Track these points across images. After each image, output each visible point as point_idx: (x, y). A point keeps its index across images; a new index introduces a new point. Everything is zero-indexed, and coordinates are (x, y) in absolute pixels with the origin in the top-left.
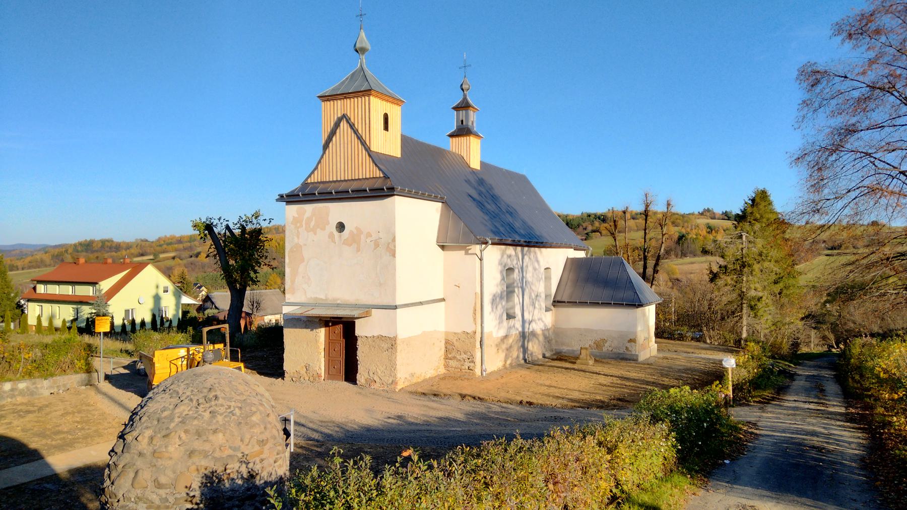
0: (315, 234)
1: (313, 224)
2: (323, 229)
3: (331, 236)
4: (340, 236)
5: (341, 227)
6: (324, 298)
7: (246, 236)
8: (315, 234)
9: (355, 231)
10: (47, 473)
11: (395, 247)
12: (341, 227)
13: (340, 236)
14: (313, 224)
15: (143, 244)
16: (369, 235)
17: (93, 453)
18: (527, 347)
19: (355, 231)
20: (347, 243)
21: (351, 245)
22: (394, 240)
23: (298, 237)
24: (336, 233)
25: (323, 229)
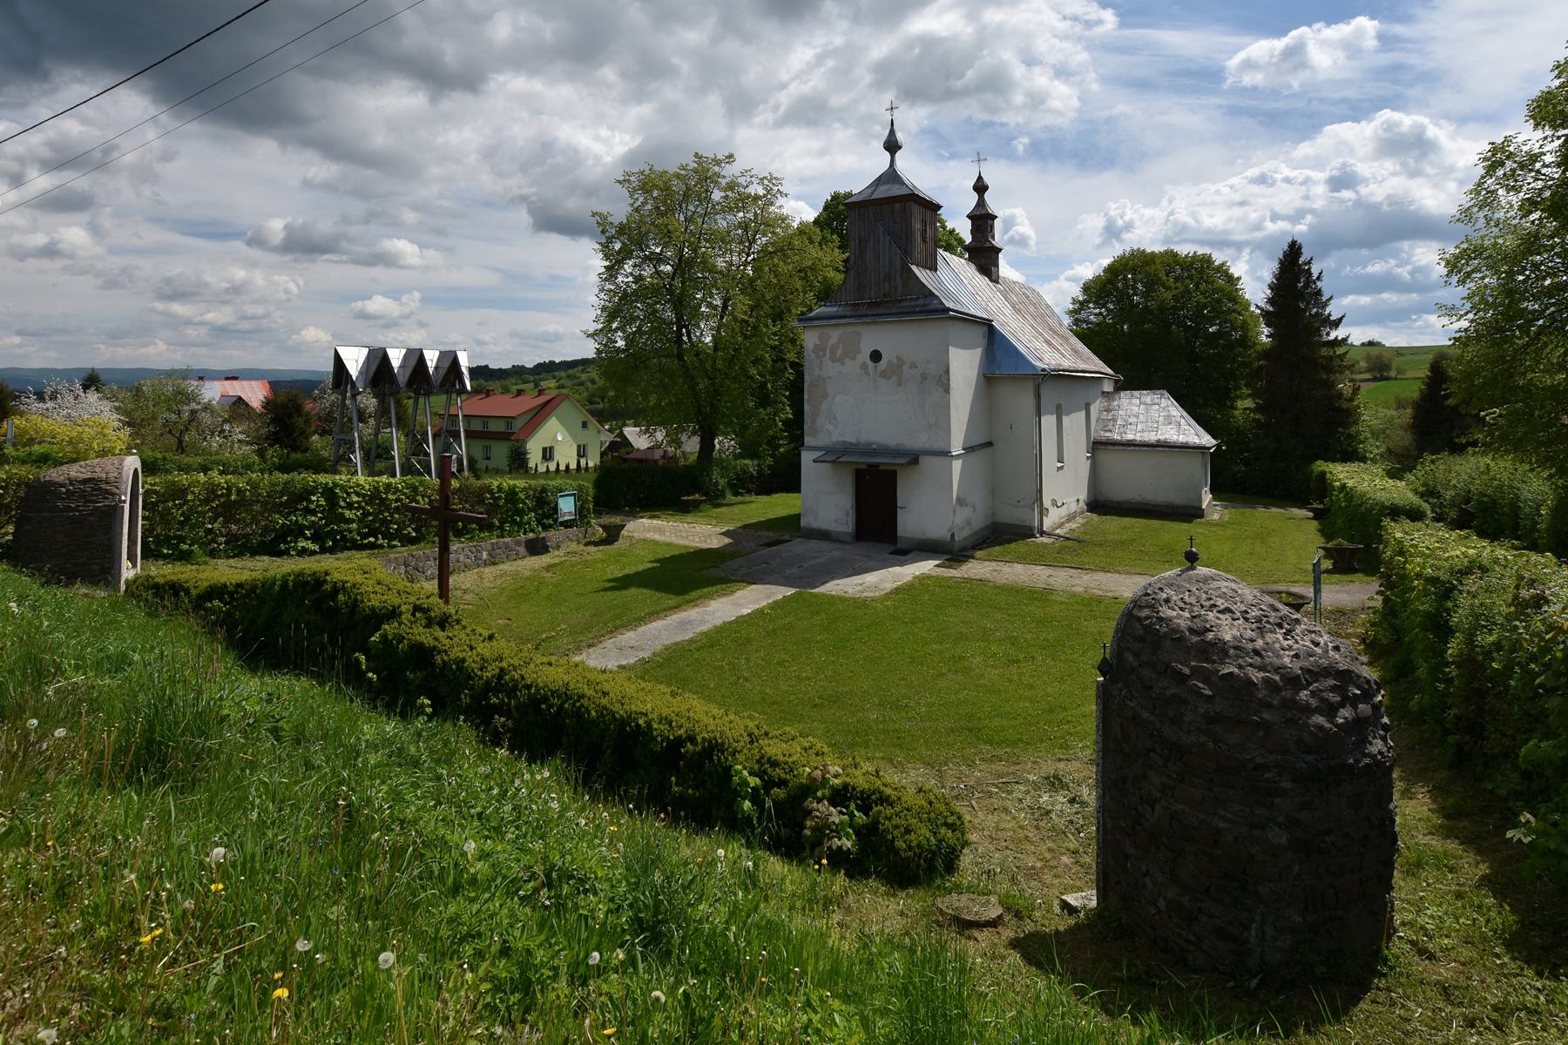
0: (843, 364)
2: (853, 359)
3: (864, 367)
4: (876, 367)
5: (876, 356)
6: (854, 441)
7: (1348, 268)
8: (843, 364)
9: (895, 361)
10: (904, 191)
11: (949, 380)
12: (876, 356)
13: (876, 367)
15: (1548, 96)
16: (913, 366)
17: (228, 571)
18: (973, 557)
19: (895, 361)
20: (884, 375)
21: (890, 377)
22: (947, 371)
23: (820, 368)
24: (871, 364)
25: (853, 359)
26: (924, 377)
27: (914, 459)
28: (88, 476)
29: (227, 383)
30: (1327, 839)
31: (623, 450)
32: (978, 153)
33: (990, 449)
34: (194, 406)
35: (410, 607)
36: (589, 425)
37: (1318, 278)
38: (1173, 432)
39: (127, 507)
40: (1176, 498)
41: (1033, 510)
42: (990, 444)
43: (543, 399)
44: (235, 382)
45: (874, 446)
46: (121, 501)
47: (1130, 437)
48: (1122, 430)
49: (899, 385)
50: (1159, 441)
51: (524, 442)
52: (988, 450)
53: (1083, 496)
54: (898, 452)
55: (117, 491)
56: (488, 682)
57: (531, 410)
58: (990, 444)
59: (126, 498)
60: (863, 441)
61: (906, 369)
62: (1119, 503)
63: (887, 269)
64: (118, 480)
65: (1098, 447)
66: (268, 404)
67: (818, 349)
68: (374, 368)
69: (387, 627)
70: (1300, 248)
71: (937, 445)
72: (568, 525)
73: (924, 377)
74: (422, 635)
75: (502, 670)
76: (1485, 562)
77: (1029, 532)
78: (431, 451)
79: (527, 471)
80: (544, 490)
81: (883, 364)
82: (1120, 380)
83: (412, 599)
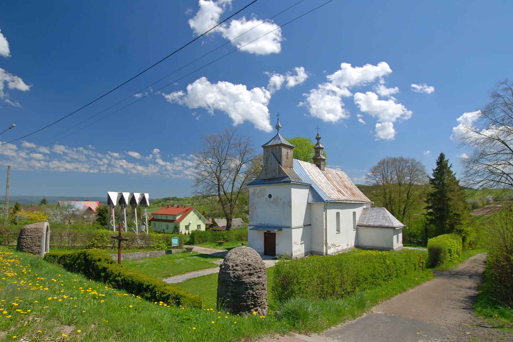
1: (259, 195)
3: (266, 199)
5: (270, 196)
9: (275, 198)
12: (270, 196)
14: (259, 195)
16: (281, 199)
19: (275, 198)
23: (254, 200)
26: (284, 203)
27: (280, 229)
28: (35, 227)
29: (86, 202)
30: (239, 295)
31: (214, 227)
32: (317, 126)
33: (310, 226)
34: (73, 209)
35: (104, 259)
36: (201, 218)
37: (450, 166)
38: (384, 222)
39: (45, 235)
40: (385, 245)
41: (323, 247)
42: (310, 225)
43: (186, 209)
44: (88, 202)
45: (269, 225)
46: (44, 234)
47: (370, 224)
48: (367, 221)
49: (277, 206)
50: (379, 225)
51: (179, 223)
52: (309, 227)
53: (353, 245)
54: (276, 227)
55: (42, 231)
56: (116, 275)
57: (183, 212)
58: (310, 225)
59: (45, 233)
60: (266, 223)
61: (279, 200)
62: (366, 246)
63: (274, 168)
64: (42, 229)
65: (358, 227)
66: (98, 209)
67: (253, 194)
68: (119, 198)
69: (157, 295)
70: (444, 155)
71: (287, 225)
72: (177, 247)
73: (284, 203)
74: (105, 265)
75: (120, 272)
76: (453, 265)
77: (321, 254)
78: (136, 224)
79: (178, 234)
80: (168, 237)
81: (272, 198)
82: (373, 204)
83: (106, 257)
